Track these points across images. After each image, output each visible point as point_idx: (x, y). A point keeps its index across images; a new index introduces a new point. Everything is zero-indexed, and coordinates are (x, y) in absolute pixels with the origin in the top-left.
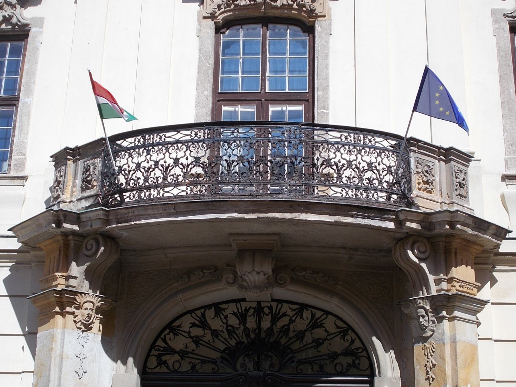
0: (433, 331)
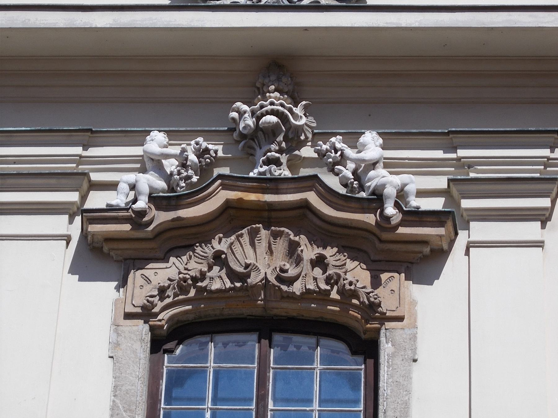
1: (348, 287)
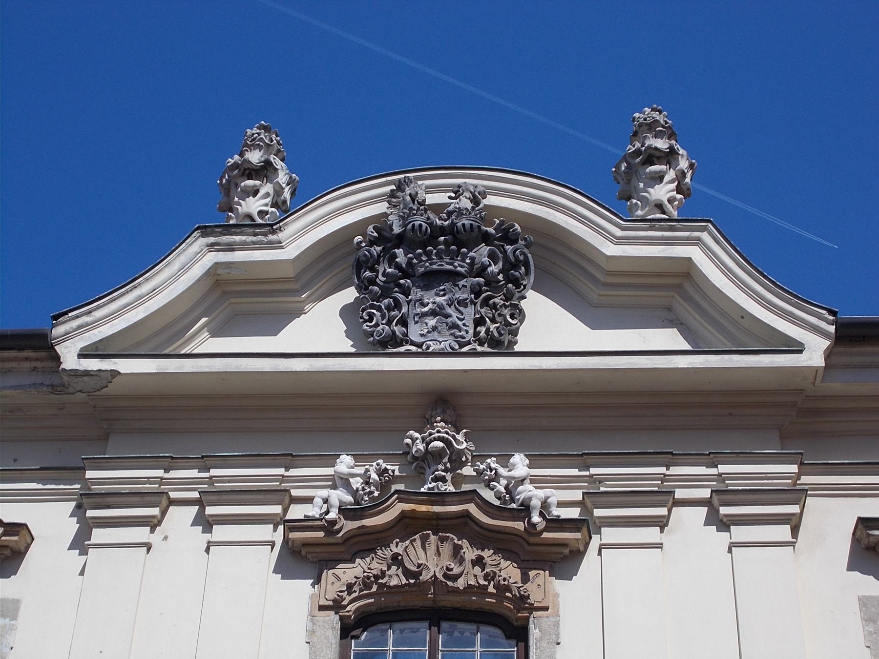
1: (502, 582)
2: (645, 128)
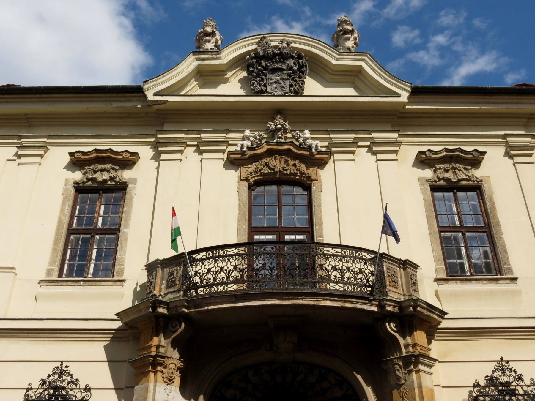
0: (405, 380)
1: (302, 172)
2: (342, 23)
